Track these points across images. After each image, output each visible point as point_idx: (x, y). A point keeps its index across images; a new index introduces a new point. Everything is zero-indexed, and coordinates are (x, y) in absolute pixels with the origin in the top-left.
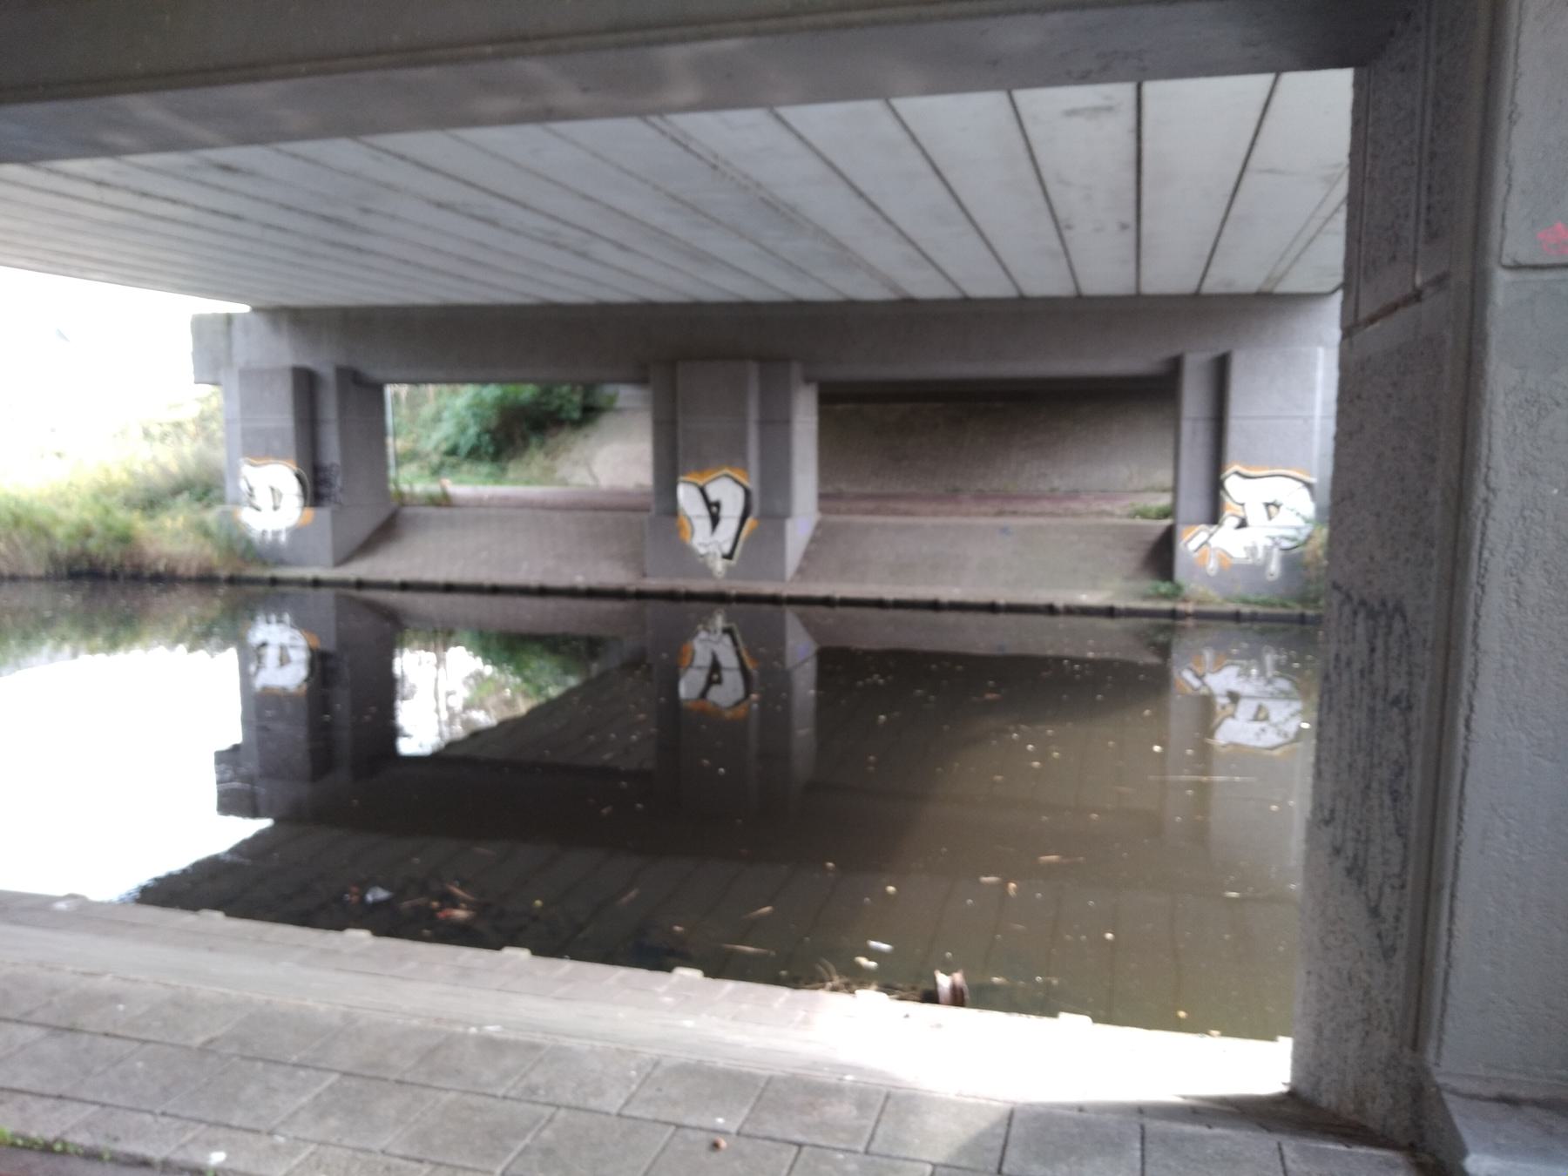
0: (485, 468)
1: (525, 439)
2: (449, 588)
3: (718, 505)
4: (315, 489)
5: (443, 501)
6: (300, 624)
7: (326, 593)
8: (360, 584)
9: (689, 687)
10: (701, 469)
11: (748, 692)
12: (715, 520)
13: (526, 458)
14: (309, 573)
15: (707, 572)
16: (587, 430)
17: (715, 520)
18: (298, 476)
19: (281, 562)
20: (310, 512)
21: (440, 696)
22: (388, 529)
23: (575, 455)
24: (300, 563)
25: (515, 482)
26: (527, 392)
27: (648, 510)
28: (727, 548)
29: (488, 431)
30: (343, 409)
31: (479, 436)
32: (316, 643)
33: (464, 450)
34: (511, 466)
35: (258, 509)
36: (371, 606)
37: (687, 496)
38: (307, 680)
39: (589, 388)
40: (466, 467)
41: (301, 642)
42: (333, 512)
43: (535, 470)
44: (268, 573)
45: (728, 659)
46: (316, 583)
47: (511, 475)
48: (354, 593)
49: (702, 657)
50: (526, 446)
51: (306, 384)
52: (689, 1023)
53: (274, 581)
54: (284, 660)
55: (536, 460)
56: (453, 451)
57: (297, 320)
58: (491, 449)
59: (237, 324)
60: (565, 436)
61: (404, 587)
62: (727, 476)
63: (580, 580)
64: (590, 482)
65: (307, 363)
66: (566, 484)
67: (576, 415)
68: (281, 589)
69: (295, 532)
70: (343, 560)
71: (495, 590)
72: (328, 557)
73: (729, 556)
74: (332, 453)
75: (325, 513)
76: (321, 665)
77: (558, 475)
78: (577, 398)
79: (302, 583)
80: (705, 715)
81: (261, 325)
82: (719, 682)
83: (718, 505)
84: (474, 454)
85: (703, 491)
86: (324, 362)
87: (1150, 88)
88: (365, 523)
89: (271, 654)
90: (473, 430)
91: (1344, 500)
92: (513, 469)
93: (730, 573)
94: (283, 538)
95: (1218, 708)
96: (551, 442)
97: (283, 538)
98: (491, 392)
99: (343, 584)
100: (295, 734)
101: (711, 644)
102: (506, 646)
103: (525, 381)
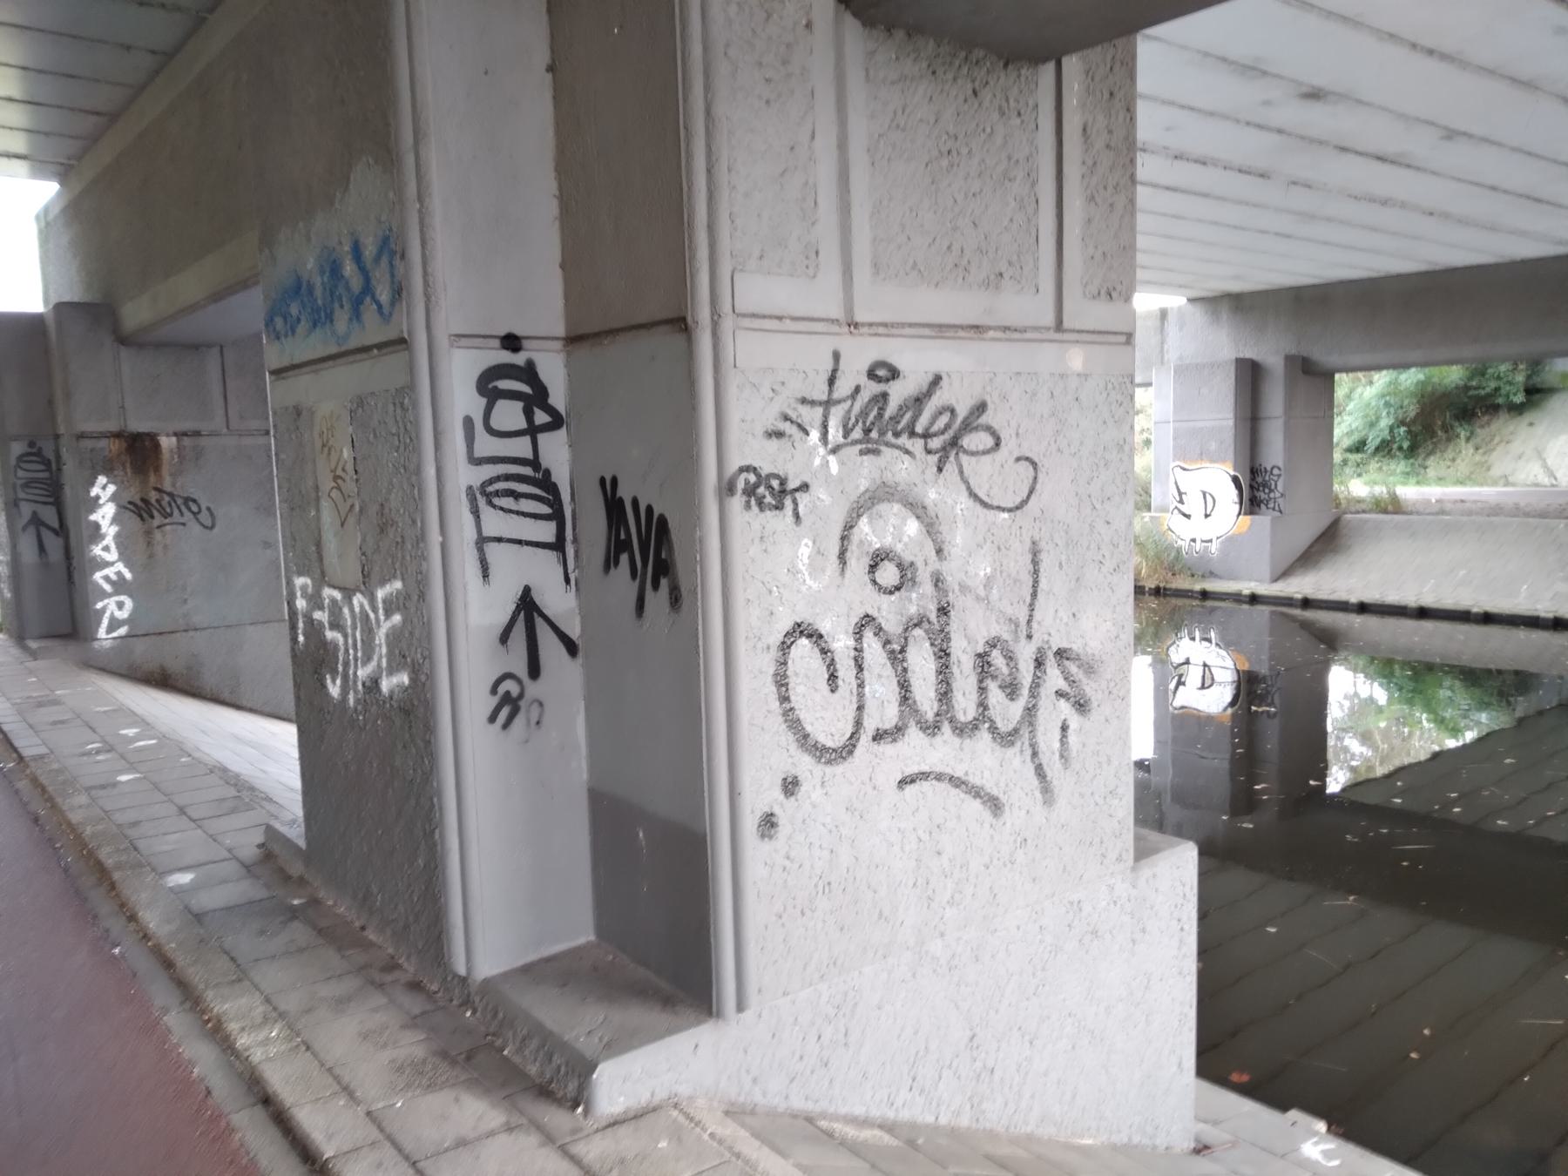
0: (1401, 466)
1: (1446, 428)
2: (1423, 613)
4: (1254, 491)
5: (1392, 506)
6: (1226, 643)
7: (1264, 610)
8: (1307, 603)
13: (1450, 454)
14: (1246, 588)
16: (1528, 417)
18: (1235, 480)
19: (1212, 575)
20: (1246, 520)
21: (1367, 726)
22: (1328, 541)
23: (1516, 446)
25: (1440, 480)
26: (1453, 375)
27: (277, 373)
29: (1402, 423)
30: (1288, 407)
31: (1391, 429)
33: (1372, 445)
34: (1431, 461)
35: (1188, 516)
36: (1306, 626)
38: (1232, 704)
39: (1536, 364)
40: (1374, 465)
41: (1230, 664)
42: (1273, 520)
43: (1462, 466)
46: (1254, 599)
47: (1431, 473)
48: (1297, 612)
50: (1451, 437)
51: (1250, 375)
52: (105, 515)
53: (1205, 595)
55: (1464, 454)
56: (1359, 447)
57: (1239, 306)
58: (1406, 445)
59: (1171, 318)
60: (1502, 425)
61: (1363, 608)
64: (1545, 480)
65: (1249, 354)
66: (1507, 484)
67: (1519, 398)
68: (1209, 603)
69: (1230, 542)
70: (1285, 574)
71: (1488, 619)
72: (1265, 569)
74: (1274, 453)
75: (1264, 520)
76: (1249, 687)
77: (1496, 471)
78: (1520, 378)
79: (1237, 598)
81: (1198, 315)
84: (1385, 449)
86: (1271, 353)
87: (1065, 61)
88: (1304, 533)
89: (1194, 676)
90: (1385, 422)
92: (1435, 466)
94: (1214, 548)
96: (1481, 433)
97: (1214, 548)
98: (1411, 378)
99: (1288, 602)
100: (1217, 763)
102: (1415, 677)
103: (1450, 362)
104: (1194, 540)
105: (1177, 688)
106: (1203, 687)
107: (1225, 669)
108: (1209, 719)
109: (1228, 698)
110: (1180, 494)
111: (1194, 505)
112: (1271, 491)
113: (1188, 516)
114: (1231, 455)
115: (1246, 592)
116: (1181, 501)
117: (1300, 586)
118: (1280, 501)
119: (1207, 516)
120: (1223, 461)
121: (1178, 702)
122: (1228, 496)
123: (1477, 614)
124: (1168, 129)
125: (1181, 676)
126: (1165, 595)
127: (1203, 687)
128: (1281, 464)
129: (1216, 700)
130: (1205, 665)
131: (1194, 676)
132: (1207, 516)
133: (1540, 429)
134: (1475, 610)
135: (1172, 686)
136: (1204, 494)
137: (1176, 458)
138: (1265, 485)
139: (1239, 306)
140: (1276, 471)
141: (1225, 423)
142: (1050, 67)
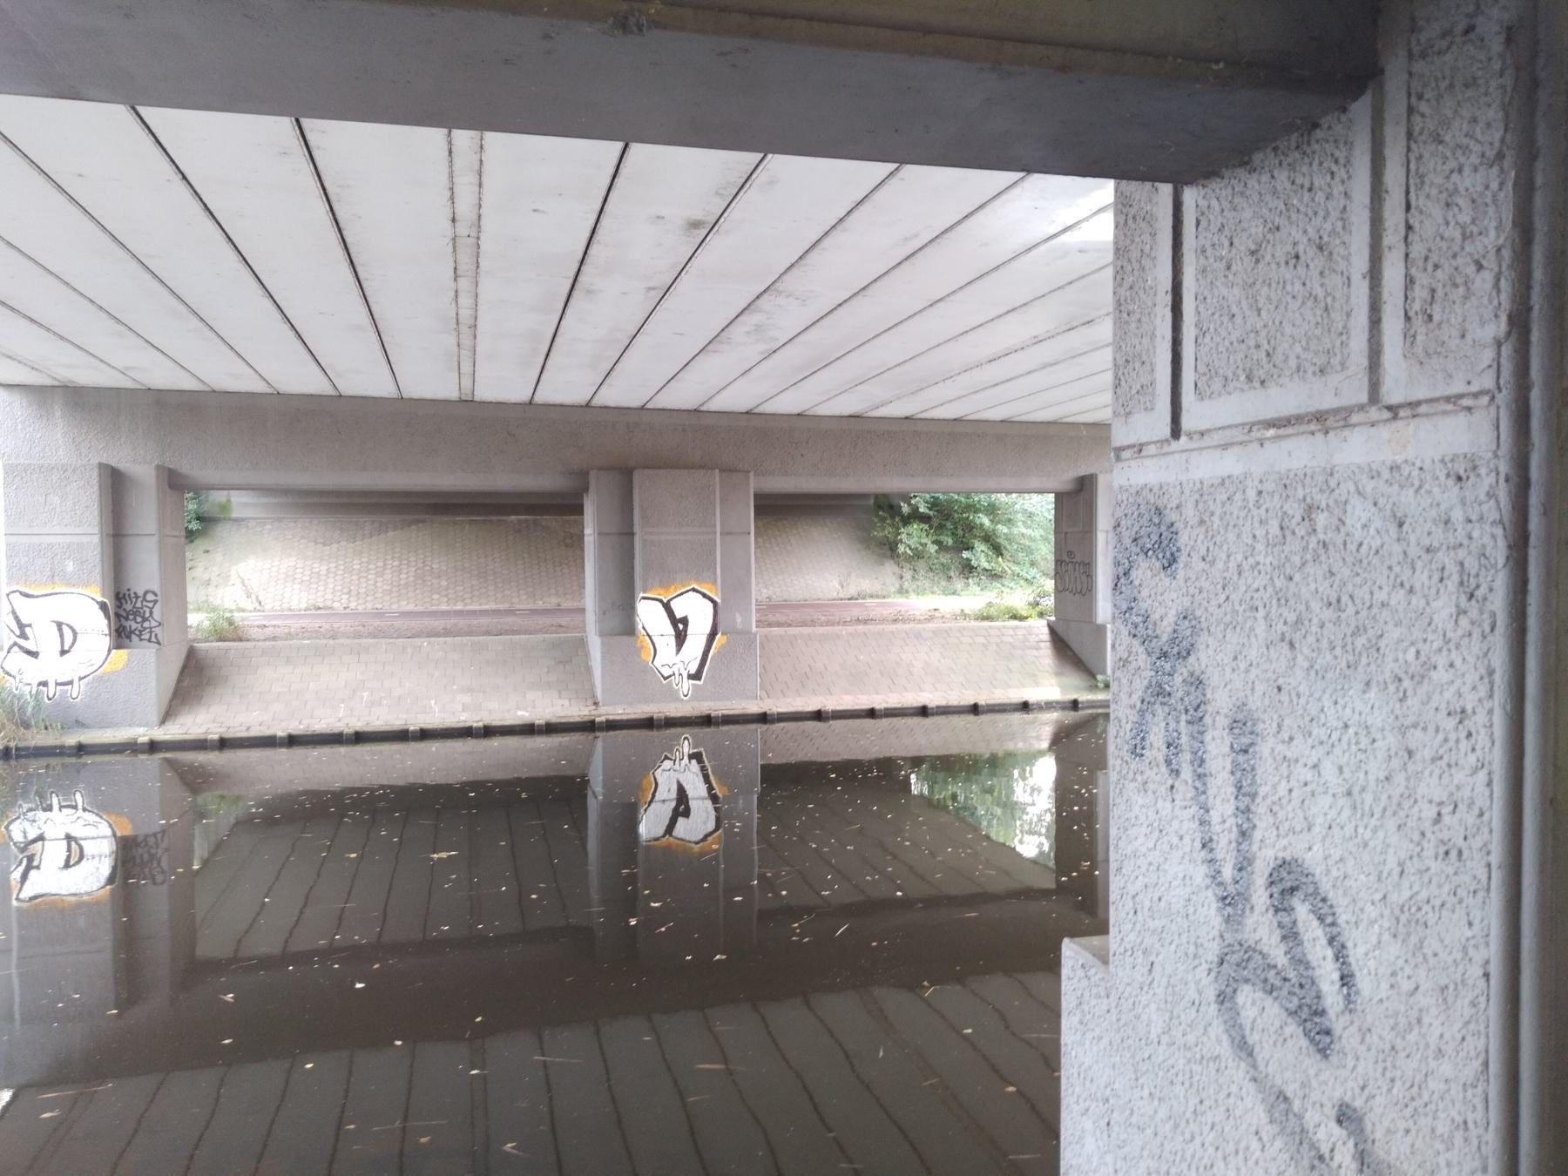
3: (685, 621)
4: (126, 619)
6: (101, 806)
9: (650, 826)
10: (665, 584)
11: (717, 828)
12: (681, 638)
15: (673, 695)
17: (681, 638)
18: (103, 606)
19: (80, 724)
20: (121, 656)
24: (102, 725)
28: (693, 669)
32: (126, 830)
35: (34, 654)
37: (649, 615)
44: (71, 740)
45: (696, 789)
49: (666, 793)
51: (115, 485)
54: (75, 854)
61: (224, 744)
62: (694, 590)
63: (522, 716)
69: (99, 681)
70: (167, 716)
71: (359, 738)
72: (154, 717)
73: (696, 676)
74: (146, 575)
76: (130, 857)
80: (668, 854)
82: (686, 813)
83: (685, 621)
85: (667, 607)
89: (54, 853)
91: (8, 880)
93: (697, 694)
95: (1490, 262)
100: (101, 952)
101: (678, 773)
104: (45, 684)
105: (24, 877)
106: (67, 865)
107: (100, 841)
108: (97, 903)
109: (105, 869)
110: (21, 626)
111: (44, 638)
112: (144, 620)
113: (34, 654)
114: (97, 575)
115: (143, 740)
116: (24, 636)
117: (197, 723)
118: (157, 630)
119: (63, 652)
120: (86, 585)
121: (28, 892)
122: (94, 626)
123: (414, 732)
124: (1463, 336)
125: (31, 859)
126: (18, 757)
127: (67, 865)
128: (156, 588)
129: (91, 877)
130: (69, 838)
131: (54, 853)
132: (63, 652)
133: (218, 557)
134: (346, 731)
135: (16, 875)
136: (59, 625)
137: (11, 578)
138: (136, 613)
139: (80, 402)
140: (150, 597)
141: (85, 539)
142: (619, 145)
